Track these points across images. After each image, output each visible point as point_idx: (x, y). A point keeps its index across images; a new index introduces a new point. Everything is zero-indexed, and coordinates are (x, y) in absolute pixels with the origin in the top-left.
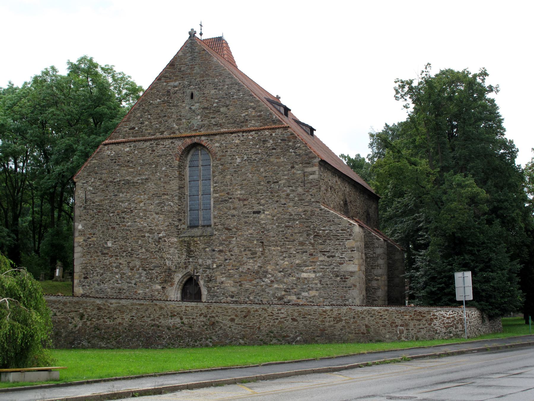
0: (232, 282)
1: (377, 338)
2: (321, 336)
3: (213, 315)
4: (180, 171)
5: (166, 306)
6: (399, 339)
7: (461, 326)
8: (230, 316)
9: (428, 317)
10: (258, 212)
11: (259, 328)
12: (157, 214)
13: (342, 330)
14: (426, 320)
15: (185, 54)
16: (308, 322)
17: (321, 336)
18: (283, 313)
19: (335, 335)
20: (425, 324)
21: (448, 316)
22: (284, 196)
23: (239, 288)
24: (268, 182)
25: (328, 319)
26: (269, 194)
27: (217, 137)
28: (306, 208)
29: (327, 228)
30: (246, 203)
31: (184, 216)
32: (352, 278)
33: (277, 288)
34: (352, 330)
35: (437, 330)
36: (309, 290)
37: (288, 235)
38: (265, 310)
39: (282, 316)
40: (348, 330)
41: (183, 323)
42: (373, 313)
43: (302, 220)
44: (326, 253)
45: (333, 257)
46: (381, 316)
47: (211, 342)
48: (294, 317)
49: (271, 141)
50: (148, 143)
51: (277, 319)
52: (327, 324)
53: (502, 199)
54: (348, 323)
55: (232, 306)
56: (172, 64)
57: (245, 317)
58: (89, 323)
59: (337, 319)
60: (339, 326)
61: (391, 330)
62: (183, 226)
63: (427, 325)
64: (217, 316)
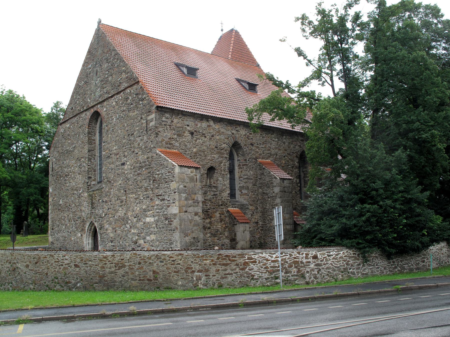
1: (165, 285)
2: (100, 282)
3: (15, 261)
4: (90, 137)
6: (196, 286)
7: (295, 270)
8: (26, 262)
9: (242, 261)
11: (47, 274)
13: (123, 276)
14: (237, 265)
16: (89, 268)
17: (100, 282)
18: (67, 259)
19: (115, 282)
20: (235, 269)
21: (273, 259)
22: (136, 146)
23: (115, 233)
25: (109, 265)
26: (129, 146)
27: (105, 103)
29: (160, 172)
31: (95, 174)
35: (254, 276)
36: (150, 234)
38: (53, 256)
39: (66, 262)
40: (131, 276)
42: (163, 257)
43: (147, 167)
44: (159, 197)
45: (163, 200)
47: (11, 286)
48: (77, 263)
51: (62, 265)
52: (108, 270)
53: (413, 120)
54: (132, 269)
55: (28, 253)
56: (89, 52)
57: (36, 263)
59: (120, 265)
61: (185, 276)
62: (93, 183)
63: (238, 270)
64: (17, 262)
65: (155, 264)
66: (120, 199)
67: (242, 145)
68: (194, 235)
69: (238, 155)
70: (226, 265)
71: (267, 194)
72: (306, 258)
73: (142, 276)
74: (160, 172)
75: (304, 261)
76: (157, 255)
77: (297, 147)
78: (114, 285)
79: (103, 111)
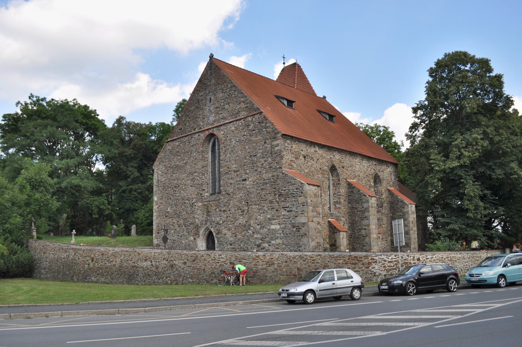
0: (230, 234)
3: (172, 259)
5: (142, 252)
9: (366, 261)
10: (245, 180)
11: (204, 270)
12: (191, 186)
13: (273, 272)
14: (363, 264)
15: (207, 72)
19: (266, 276)
20: (362, 268)
21: (389, 260)
22: (260, 166)
24: (251, 156)
26: (251, 165)
27: (222, 128)
28: (274, 174)
29: (287, 188)
30: (238, 173)
32: (304, 228)
33: (256, 238)
34: (283, 272)
35: (376, 273)
36: (276, 239)
37: (263, 196)
38: (209, 255)
39: (222, 260)
40: (279, 272)
41: (152, 265)
42: (305, 257)
43: (271, 184)
44: (286, 209)
45: (291, 211)
46: (314, 260)
49: (252, 125)
50: (187, 138)
52: (260, 267)
54: (280, 266)
57: (194, 261)
58: (96, 264)
59: (270, 263)
60: (271, 268)
63: (364, 268)
65: (299, 263)
66: (241, 209)
67: (337, 168)
68: (317, 240)
69: (332, 176)
70: (355, 264)
71: (356, 208)
72: (413, 260)
73: (288, 272)
74: (287, 188)
75: (412, 262)
76: (301, 256)
77: (372, 170)
78: (266, 279)
79: (220, 134)
